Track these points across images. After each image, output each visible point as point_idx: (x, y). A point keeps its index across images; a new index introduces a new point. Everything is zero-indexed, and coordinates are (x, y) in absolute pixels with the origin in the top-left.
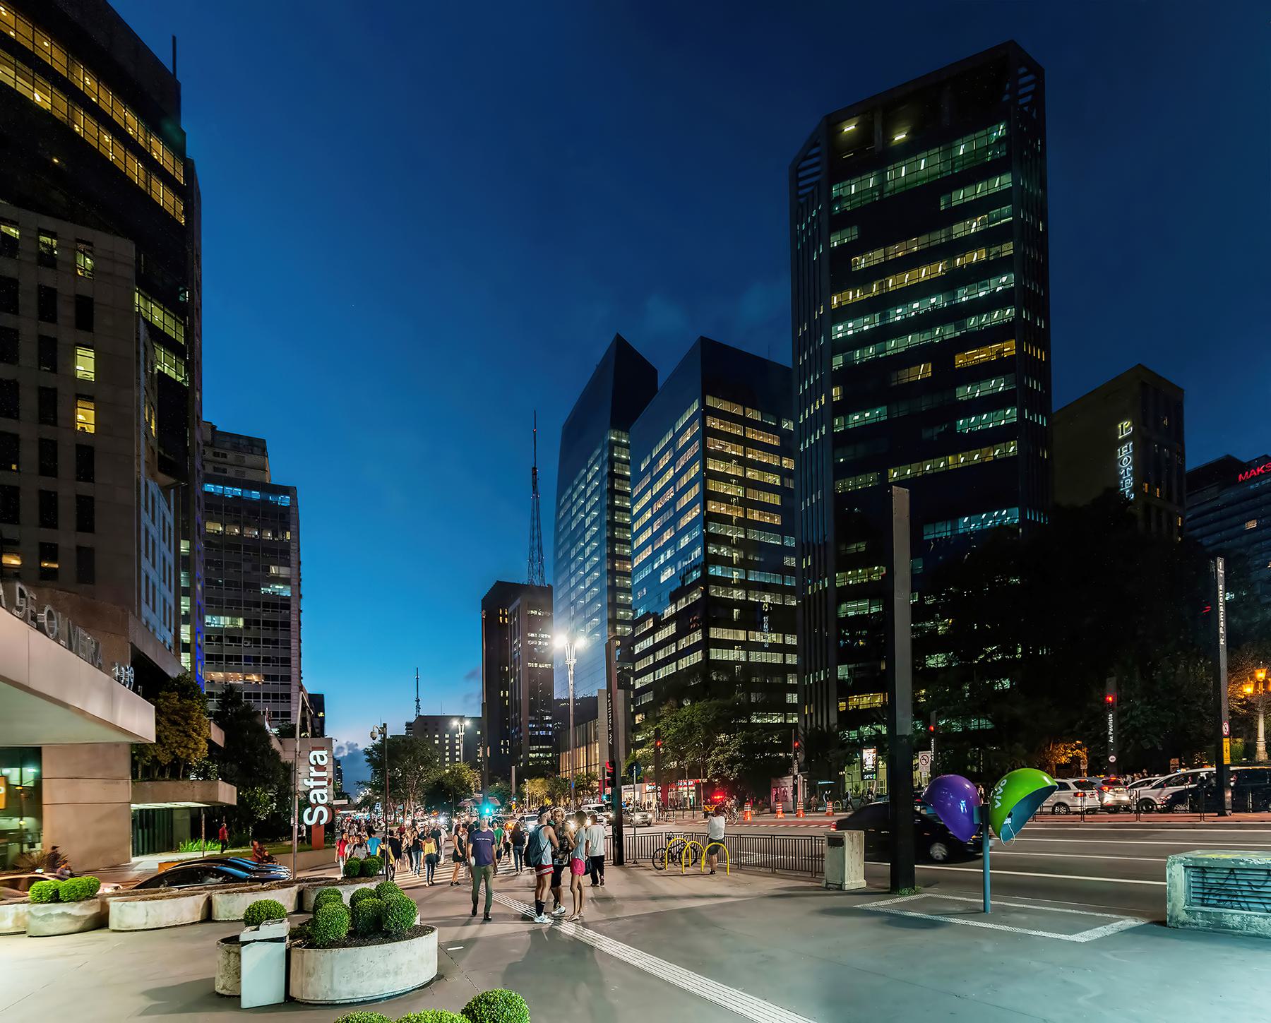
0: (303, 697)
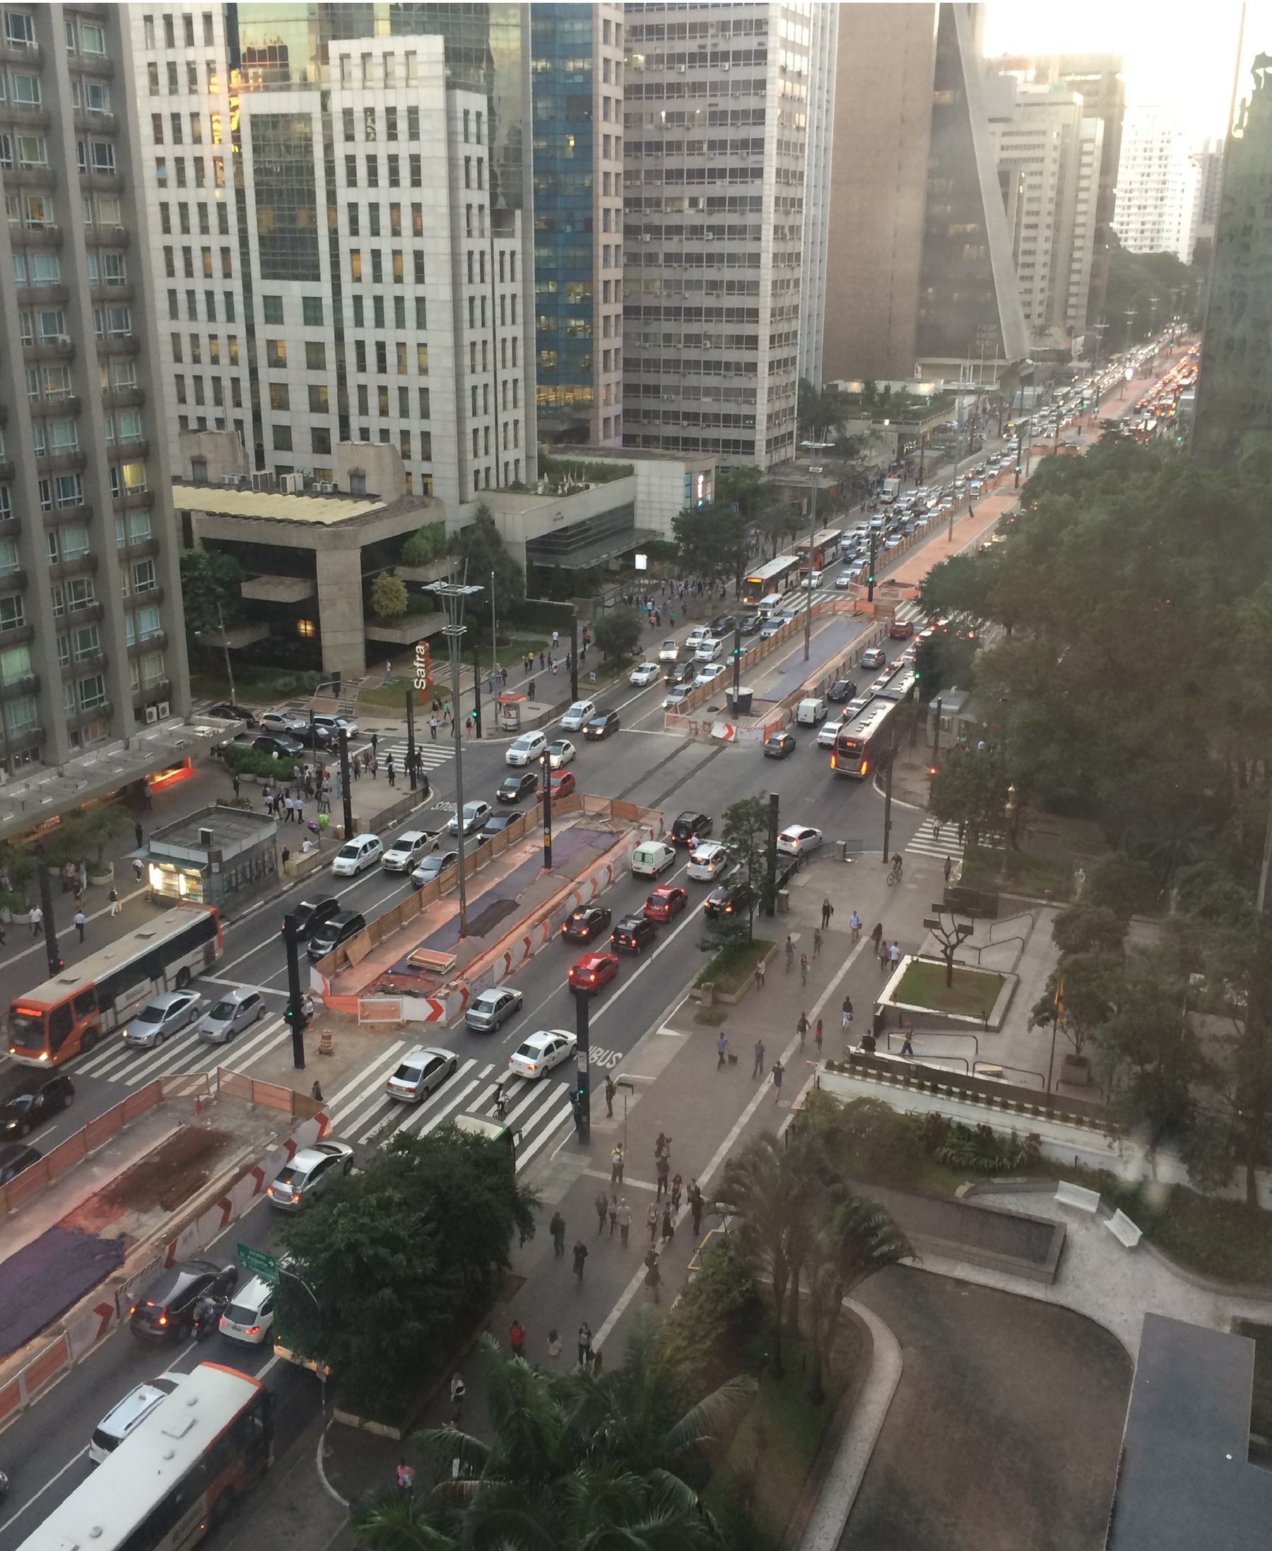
0: (186, 1001)
